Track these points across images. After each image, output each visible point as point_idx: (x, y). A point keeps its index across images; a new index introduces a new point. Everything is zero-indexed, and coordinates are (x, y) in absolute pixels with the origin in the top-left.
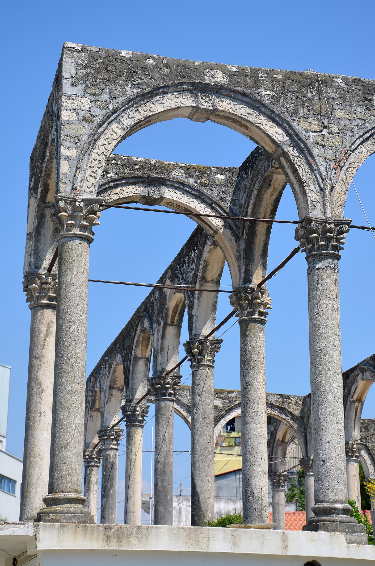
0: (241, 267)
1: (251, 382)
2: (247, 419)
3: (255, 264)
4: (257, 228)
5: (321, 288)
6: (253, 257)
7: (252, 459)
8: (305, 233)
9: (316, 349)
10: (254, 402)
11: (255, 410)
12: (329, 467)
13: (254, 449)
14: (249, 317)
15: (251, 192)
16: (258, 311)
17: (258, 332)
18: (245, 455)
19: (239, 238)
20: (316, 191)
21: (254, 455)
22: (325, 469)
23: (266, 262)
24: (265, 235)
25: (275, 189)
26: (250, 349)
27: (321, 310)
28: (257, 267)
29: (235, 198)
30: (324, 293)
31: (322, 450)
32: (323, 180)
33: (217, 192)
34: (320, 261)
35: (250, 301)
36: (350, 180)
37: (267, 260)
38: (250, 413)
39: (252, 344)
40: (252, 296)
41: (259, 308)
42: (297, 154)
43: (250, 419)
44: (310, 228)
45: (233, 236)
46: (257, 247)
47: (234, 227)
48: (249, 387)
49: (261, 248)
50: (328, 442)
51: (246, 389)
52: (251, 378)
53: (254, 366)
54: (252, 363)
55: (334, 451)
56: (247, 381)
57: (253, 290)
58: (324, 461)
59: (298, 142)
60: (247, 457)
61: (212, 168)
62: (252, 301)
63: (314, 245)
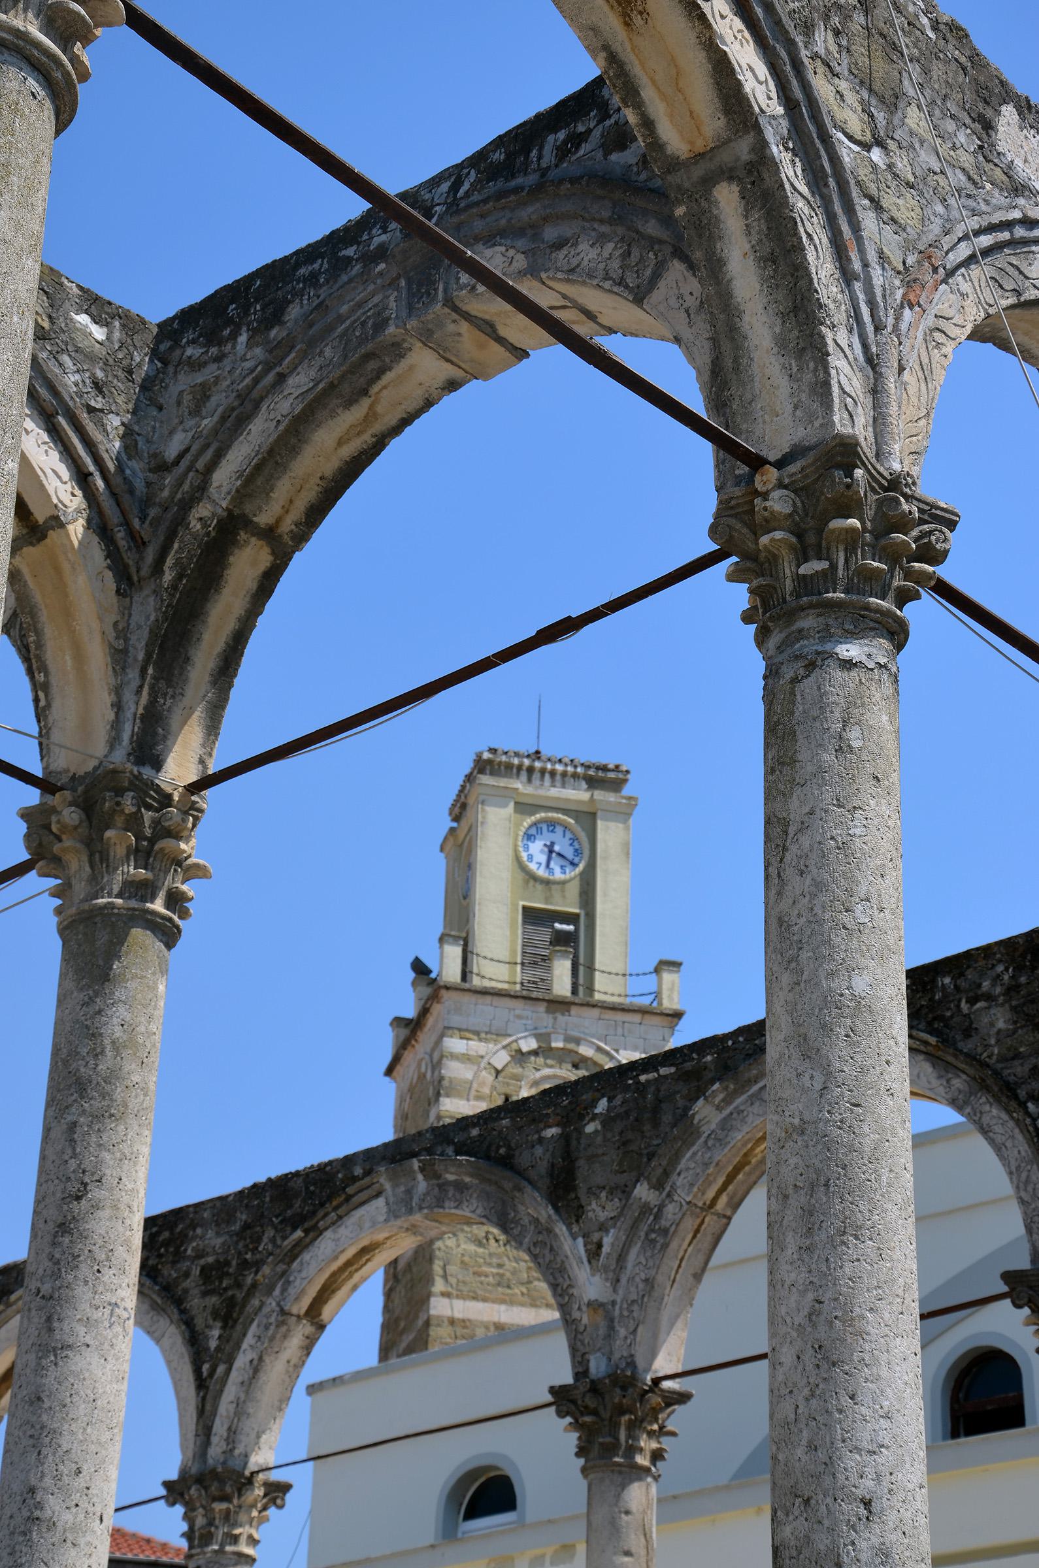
0: (128, 696)
1: (108, 1172)
2: (66, 1328)
3: (186, 701)
4: (232, 559)
5: (861, 743)
6: (183, 670)
7: (67, 1518)
8: (795, 511)
9: (830, 990)
10: (108, 1259)
11: (108, 1297)
12: (893, 1537)
13: (79, 1472)
14: (133, 904)
15: (248, 406)
16: (165, 888)
17: (154, 974)
18: (32, 1491)
19: (130, 583)
20: (856, 359)
21: (76, 1497)
22: (876, 1541)
23: (223, 708)
24: (248, 599)
25: (371, 416)
26: (118, 1032)
27: (858, 831)
28: (189, 716)
29: (136, 428)
30: (870, 770)
31: (858, 1450)
32: (878, 329)
33: (77, 377)
34: (852, 635)
35: (146, 838)
36: (940, 376)
37: (226, 699)
38: (85, 1306)
39: (128, 1017)
40: (156, 823)
41: (170, 877)
42: (804, 189)
43: (81, 1330)
44: (848, 486)
45: (109, 567)
46: (207, 637)
47: (120, 535)
48: (95, 1193)
49: (220, 646)
50: (887, 1417)
51: (78, 1198)
52: (106, 1156)
53: (126, 1106)
54: (119, 1094)
55: (908, 1465)
56: (86, 1164)
57: (166, 800)
58: (867, 1504)
59: (813, 142)
60: (39, 1506)
61: (66, 282)
62: (152, 841)
63: (834, 566)
